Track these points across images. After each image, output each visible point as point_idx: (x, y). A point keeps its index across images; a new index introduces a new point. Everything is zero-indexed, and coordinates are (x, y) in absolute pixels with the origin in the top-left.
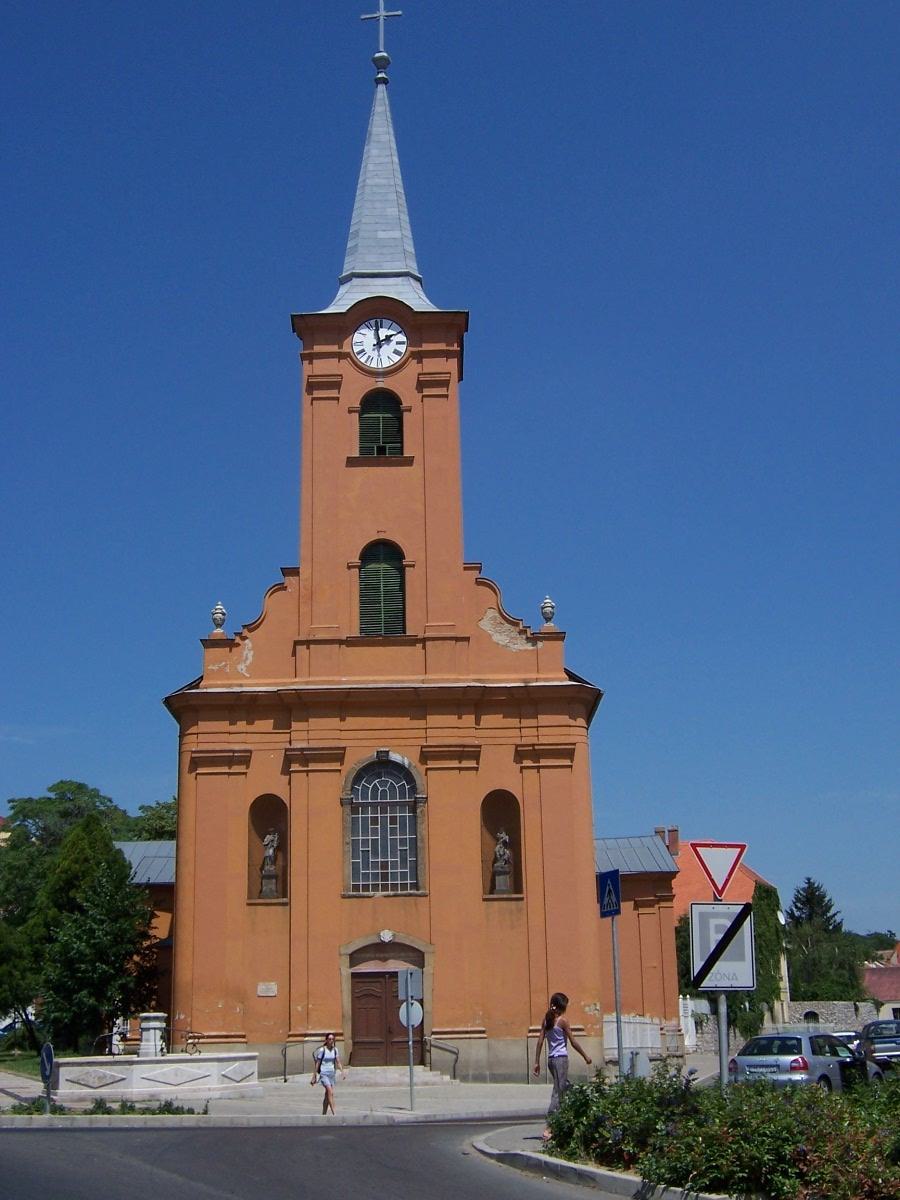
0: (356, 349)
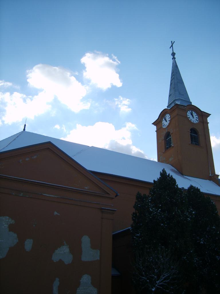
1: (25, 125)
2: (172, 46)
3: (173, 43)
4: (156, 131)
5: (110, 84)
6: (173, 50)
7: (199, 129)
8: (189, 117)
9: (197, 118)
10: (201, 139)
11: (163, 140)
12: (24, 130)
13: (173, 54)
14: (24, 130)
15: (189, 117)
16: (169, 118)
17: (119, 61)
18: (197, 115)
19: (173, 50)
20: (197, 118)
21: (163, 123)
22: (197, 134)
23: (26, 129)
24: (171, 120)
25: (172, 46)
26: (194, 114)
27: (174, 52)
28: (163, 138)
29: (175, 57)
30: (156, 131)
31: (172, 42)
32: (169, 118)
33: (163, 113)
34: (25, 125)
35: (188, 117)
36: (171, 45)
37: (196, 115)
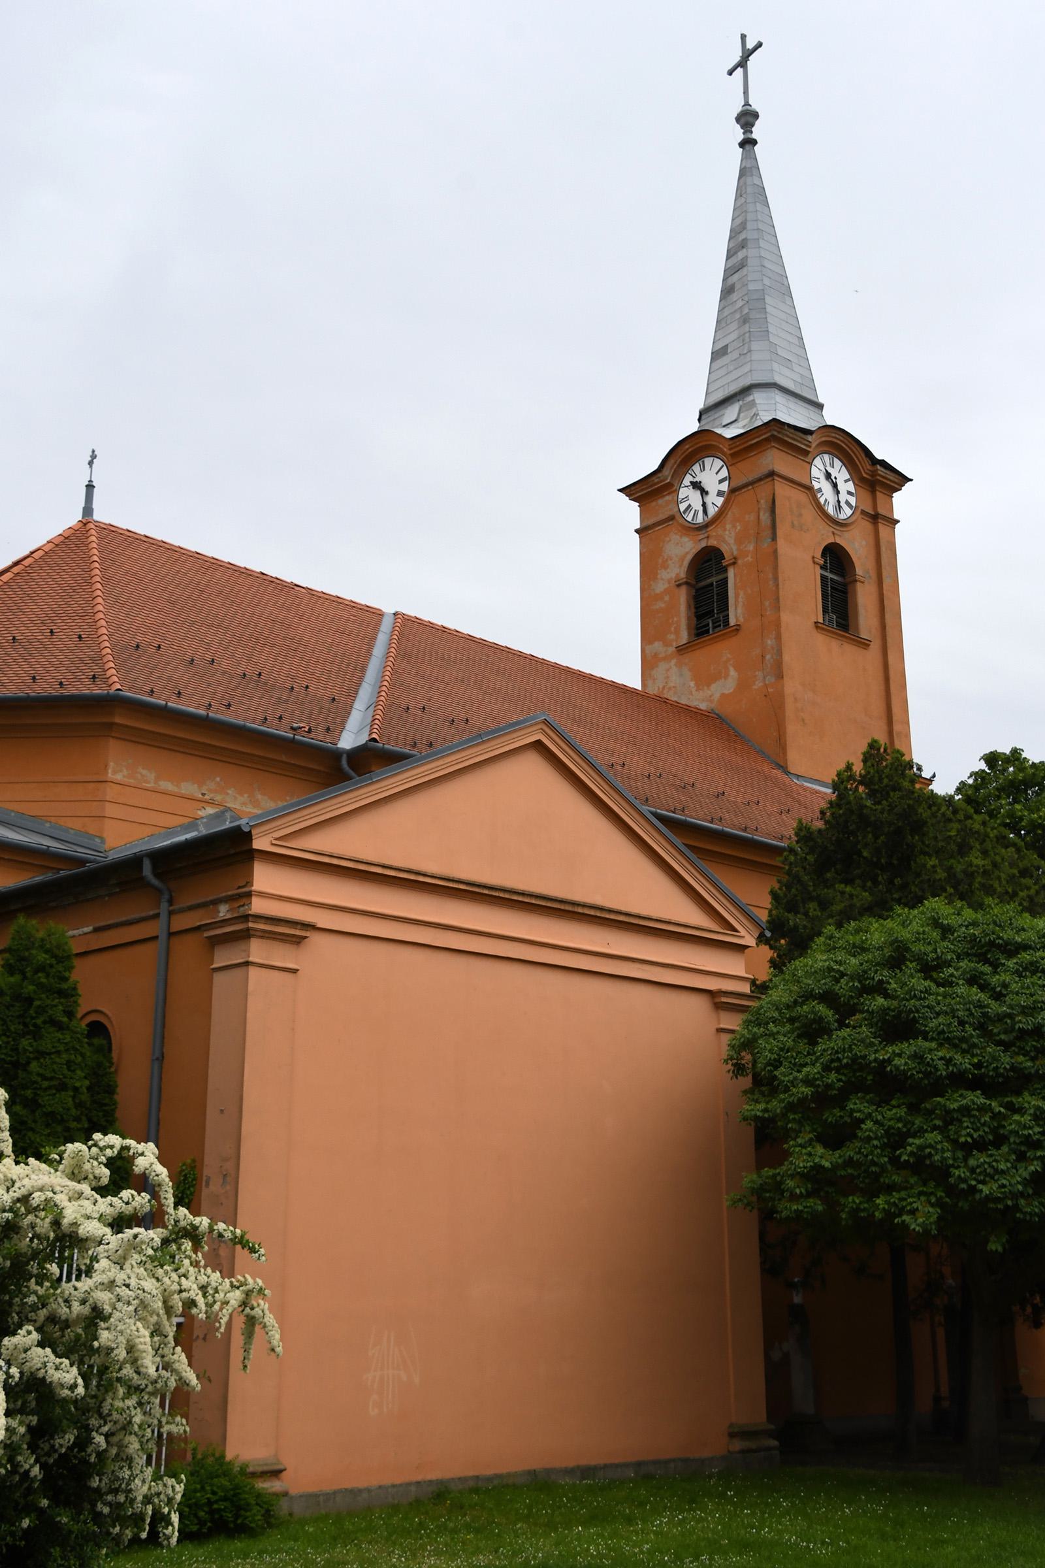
0: (682, 507)
1: (90, 487)
2: (743, 63)
3: (750, 45)
4: (637, 531)
5: (269, 1355)
6: (746, 92)
7: (857, 546)
8: (820, 490)
9: (849, 493)
10: (864, 598)
11: (679, 586)
12: (88, 510)
13: (747, 118)
14: (88, 510)
15: (820, 490)
16: (721, 481)
17: (178, 1531)
18: (852, 479)
19: (746, 92)
20: (849, 493)
21: (681, 496)
22: (842, 575)
23: (95, 506)
24: (733, 491)
25: (743, 63)
26: (841, 474)
27: (755, 105)
28: (683, 575)
29: (757, 132)
30: (637, 531)
31: (743, 37)
32: (721, 481)
33: (679, 451)
34: (90, 487)
35: (816, 486)
36: (737, 57)
37: (848, 477)
